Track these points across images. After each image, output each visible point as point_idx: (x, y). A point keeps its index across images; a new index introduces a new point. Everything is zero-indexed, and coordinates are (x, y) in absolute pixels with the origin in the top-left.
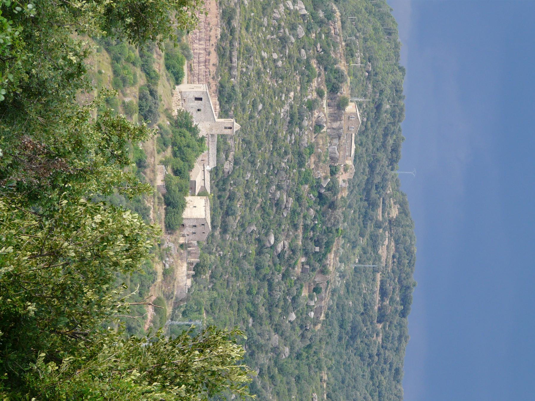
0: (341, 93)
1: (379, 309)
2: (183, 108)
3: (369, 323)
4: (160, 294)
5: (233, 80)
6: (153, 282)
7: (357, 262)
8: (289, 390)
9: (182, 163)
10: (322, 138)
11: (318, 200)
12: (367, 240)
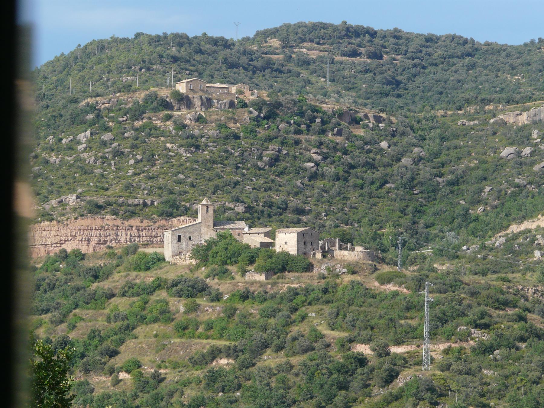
0: (167, 97)
1: (369, 57)
2: (188, 254)
3: (384, 68)
4: (372, 277)
5: (155, 204)
6: (362, 285)
7: (324, 80)
8: (456, 148)
9: (242, 256)
10: (210, 116)
11: (271, 120)
12: (302, 69)
